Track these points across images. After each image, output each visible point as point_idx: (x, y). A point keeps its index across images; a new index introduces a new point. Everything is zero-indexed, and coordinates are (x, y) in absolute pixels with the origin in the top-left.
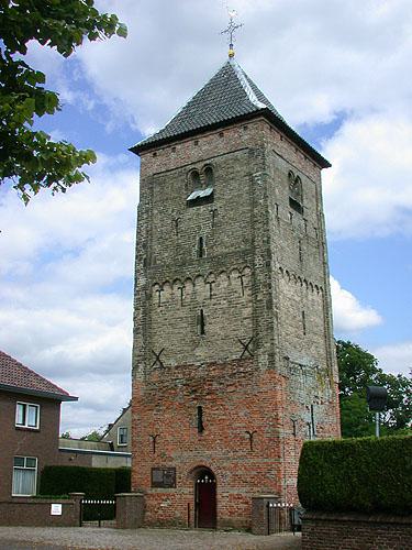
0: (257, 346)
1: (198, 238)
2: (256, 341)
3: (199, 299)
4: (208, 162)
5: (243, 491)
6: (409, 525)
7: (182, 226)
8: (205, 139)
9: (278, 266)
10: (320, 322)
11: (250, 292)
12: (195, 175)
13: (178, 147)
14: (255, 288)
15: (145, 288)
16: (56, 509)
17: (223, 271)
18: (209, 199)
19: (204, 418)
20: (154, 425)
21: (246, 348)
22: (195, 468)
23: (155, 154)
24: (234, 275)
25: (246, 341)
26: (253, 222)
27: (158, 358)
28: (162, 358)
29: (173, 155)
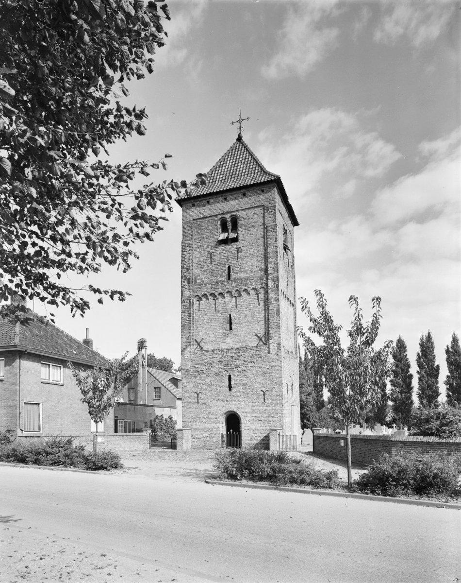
2: (267, 336)
4: (234, 214)
5: (258, 426)
6: (458, 508)
19: (232, 382)
20: (198, 386)
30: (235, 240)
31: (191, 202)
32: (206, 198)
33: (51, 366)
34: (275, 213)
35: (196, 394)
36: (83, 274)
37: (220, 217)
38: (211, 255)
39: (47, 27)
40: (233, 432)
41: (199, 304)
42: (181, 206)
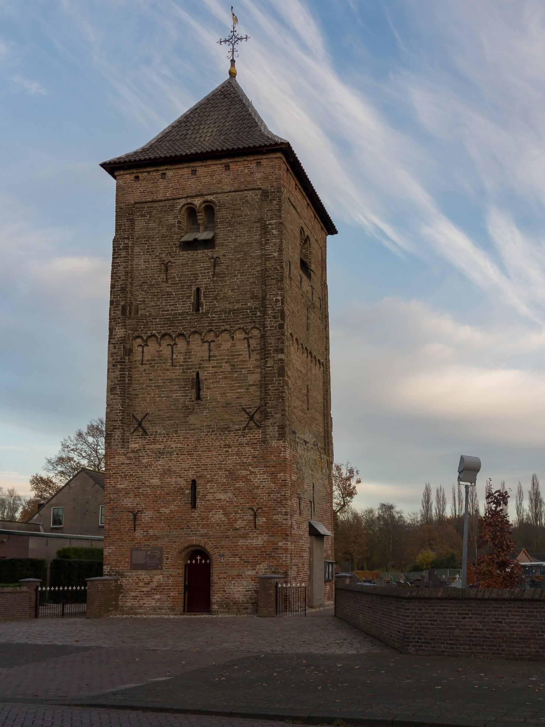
0: (266, 415)
1: (194, 289)
3: (195, 360)
4: (210, 198)
7: (174, 272)
8: (205, 169)
9: (290, 331)
10: (320, 399)
11: (258, 357)
12: (192, 212)
13: (170, 173)
14: (264, 353)
15: (123, 341)
16: (527, 569)
17: (226, 330)
18: (209, 244)
21: (251, 418)
22: (188, 547)
23: (137, 178)
24: (239, 335)
25: (252, 411)
26: (264, 277)
27: (140, 424)
28: (145, 424)
29: (162, 183)
30: (209, 244)
31: (133, 173)
32: (160, 168)
34: (280, 204)
35: (131, 514)
37: (183, 201)
39: (405, 640)
40: (201, 560)
41: (143, 352)
42: (115, 177)
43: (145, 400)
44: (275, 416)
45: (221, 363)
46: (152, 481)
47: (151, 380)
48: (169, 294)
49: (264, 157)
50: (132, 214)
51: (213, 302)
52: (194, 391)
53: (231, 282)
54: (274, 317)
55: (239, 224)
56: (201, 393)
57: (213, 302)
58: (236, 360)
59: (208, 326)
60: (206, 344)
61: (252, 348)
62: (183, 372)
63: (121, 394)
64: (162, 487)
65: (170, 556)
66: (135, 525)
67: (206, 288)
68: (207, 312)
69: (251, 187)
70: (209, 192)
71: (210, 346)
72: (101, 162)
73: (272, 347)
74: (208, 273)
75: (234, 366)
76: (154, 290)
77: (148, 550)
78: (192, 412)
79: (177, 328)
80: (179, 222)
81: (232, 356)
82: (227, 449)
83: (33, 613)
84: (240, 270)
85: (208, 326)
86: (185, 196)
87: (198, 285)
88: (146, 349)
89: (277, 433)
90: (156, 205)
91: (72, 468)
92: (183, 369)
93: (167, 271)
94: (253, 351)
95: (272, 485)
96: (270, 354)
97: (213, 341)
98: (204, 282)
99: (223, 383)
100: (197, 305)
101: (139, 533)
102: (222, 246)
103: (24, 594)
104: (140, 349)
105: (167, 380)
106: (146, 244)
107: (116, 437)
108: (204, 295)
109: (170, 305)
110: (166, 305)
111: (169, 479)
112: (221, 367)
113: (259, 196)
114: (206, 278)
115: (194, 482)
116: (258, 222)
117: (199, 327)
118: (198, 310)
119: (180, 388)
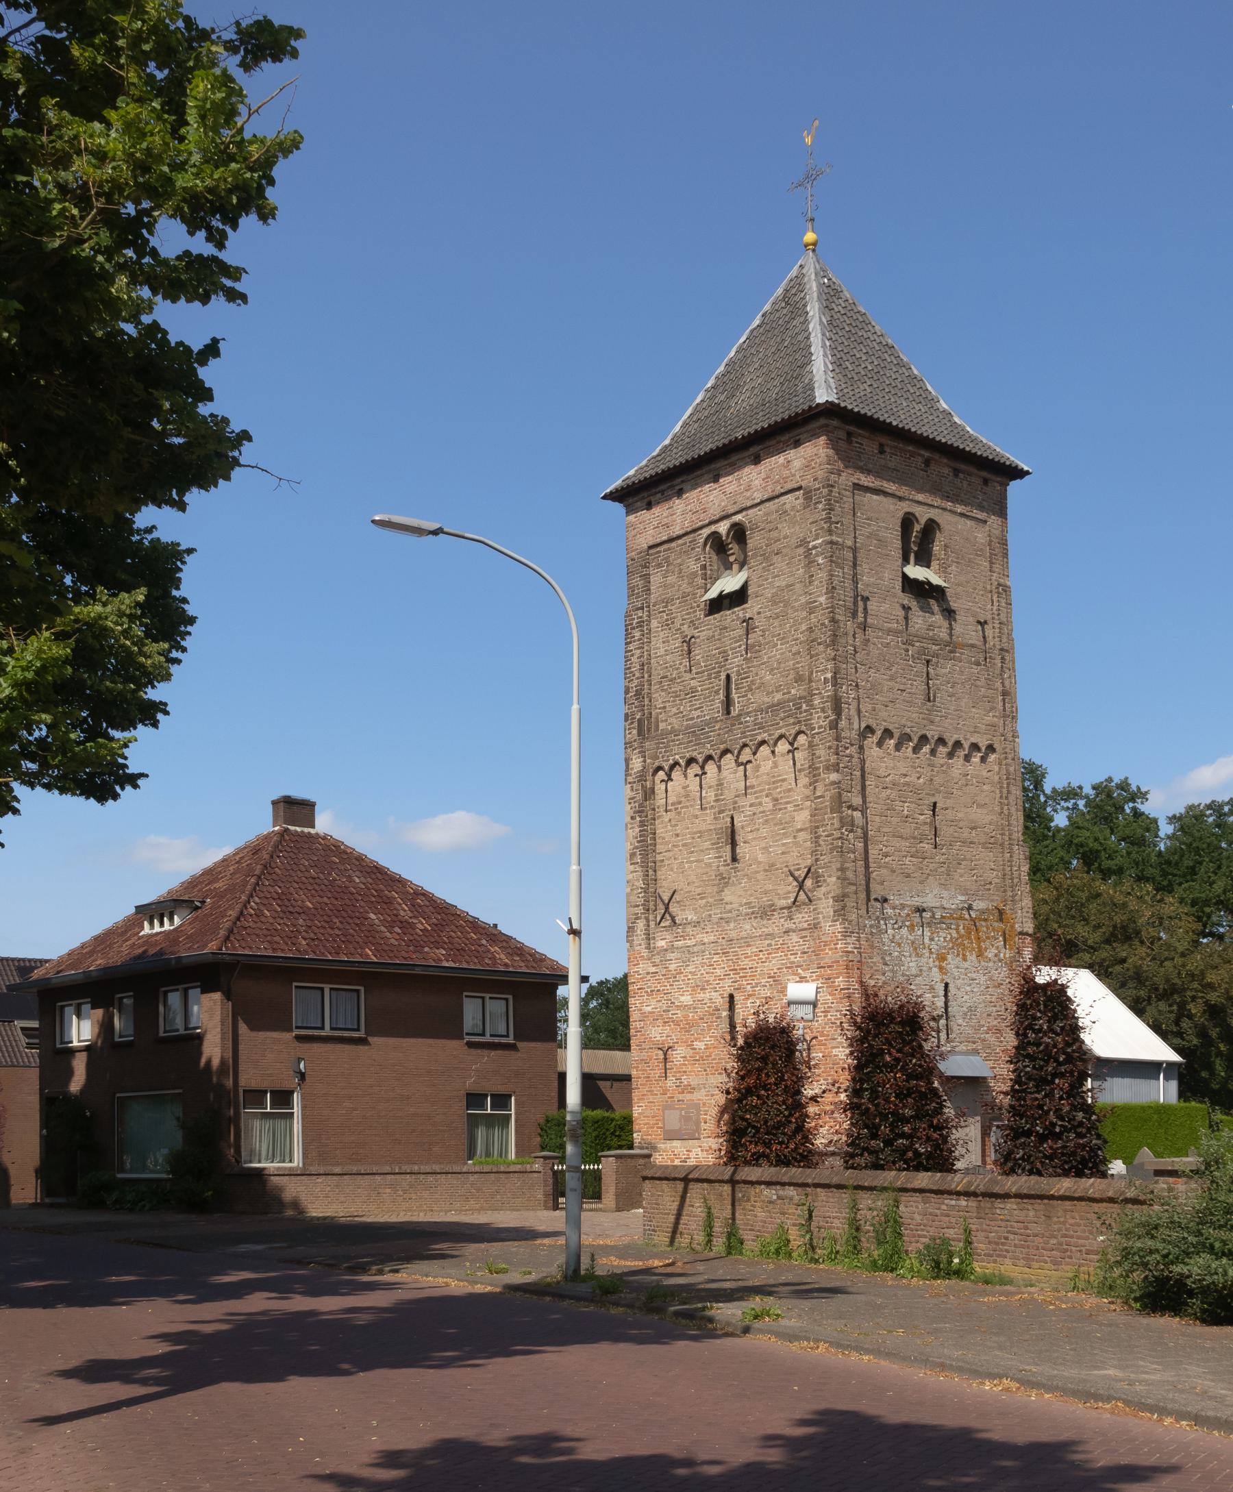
1: (723, 677)
21: (801, 886)
31: (643, 498)
32: (674, 483)
33: (487, 1000)
36: (266, 214)
37: (706, 532)
38: (689, 646)
41: (666, 791)
43: (672, 870)
44: (829, 880)
45: (761, 796)
46: (682, 999)
47: (677, 835)
48: (694, 690)
49: (803, 430)
50: (646, 567)
51: (746, 696)
52: (729, 848)
53: (769, 658)
54: (823, 710)
55: (777, 554)
56: (738, 851)
57: (746, 696)
58: (779, 790)
59: (740, 738)
60: (742, 768)
61: (798, 765)
62: (715, 818)
63: (642, 862)
64: (695, 1008)
65: (708, 1117)
66: (666, 1069)
67: (739, 674)
68: (740, 715)
69: (789, 486)
70: (736, 508)
71: (745, 771)
72: (17, 817)
73: (821, 762)
74: (740, 646)
75: (777, 800)
76: (675, 688)
77: (683, 1109)
78: (727, 883)
79: (704, 747)
80: (704, 567)
81: (774, 783)
82: (769, 942)
83: (551, 1204)
84: (779, 634)
85: (740, 738)
86: (707, 521)
87: (728, 669)
88: (670, 784)
89: (832, 910)
90: (673, 544)
91: (1112, 901)
92: (714, 814)
93: (690, 652)
94: (800, 771)
95: (829, 997)
96: (820, 775)
97: (750, 762)
98: (735, 663)
99: (764, 832)
100: (728, 703)
101: (670, 1083)
102: (757, 596)
103: (536, 1175)
104: (663, 786)
105: (695, 833)
106: (664, 611)
107: (639, 932)
108: (736, 685)
109: (696, 710)
110: (691, 711)
111: (702, 995)
112: (760, 804)
113: (801, 501)
114: (737, 657)
115: (731, 997)
116: (801, 546)
117: (731, 740)
118: (728, 713)
119: (713, 844)
